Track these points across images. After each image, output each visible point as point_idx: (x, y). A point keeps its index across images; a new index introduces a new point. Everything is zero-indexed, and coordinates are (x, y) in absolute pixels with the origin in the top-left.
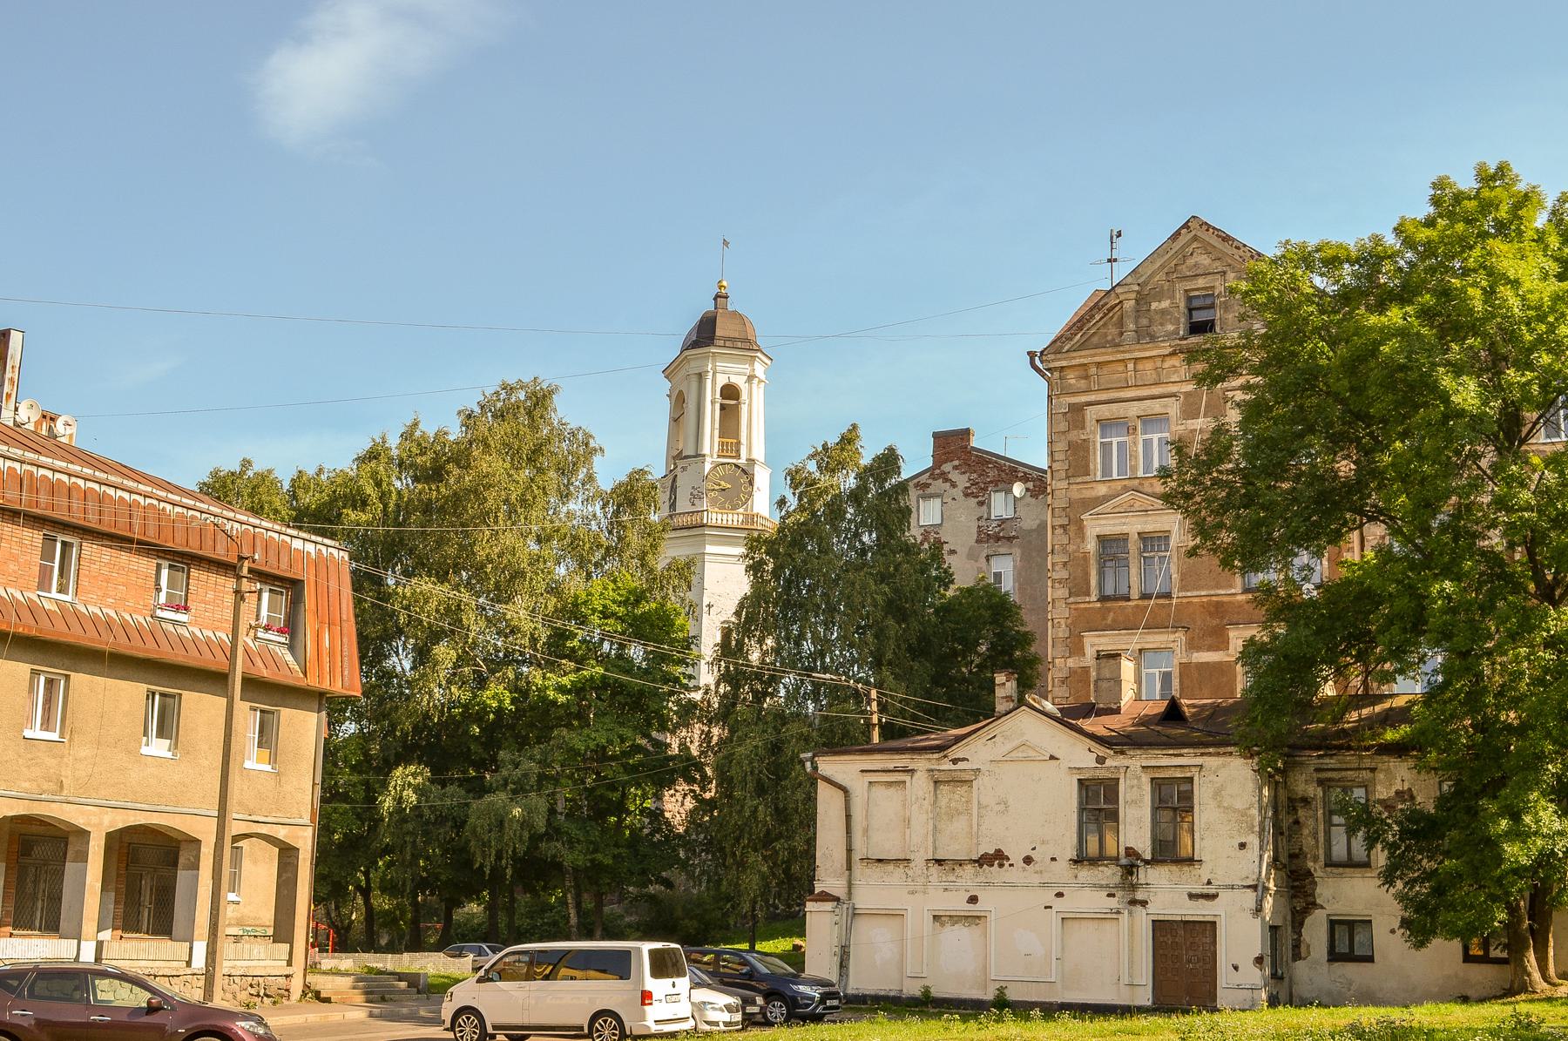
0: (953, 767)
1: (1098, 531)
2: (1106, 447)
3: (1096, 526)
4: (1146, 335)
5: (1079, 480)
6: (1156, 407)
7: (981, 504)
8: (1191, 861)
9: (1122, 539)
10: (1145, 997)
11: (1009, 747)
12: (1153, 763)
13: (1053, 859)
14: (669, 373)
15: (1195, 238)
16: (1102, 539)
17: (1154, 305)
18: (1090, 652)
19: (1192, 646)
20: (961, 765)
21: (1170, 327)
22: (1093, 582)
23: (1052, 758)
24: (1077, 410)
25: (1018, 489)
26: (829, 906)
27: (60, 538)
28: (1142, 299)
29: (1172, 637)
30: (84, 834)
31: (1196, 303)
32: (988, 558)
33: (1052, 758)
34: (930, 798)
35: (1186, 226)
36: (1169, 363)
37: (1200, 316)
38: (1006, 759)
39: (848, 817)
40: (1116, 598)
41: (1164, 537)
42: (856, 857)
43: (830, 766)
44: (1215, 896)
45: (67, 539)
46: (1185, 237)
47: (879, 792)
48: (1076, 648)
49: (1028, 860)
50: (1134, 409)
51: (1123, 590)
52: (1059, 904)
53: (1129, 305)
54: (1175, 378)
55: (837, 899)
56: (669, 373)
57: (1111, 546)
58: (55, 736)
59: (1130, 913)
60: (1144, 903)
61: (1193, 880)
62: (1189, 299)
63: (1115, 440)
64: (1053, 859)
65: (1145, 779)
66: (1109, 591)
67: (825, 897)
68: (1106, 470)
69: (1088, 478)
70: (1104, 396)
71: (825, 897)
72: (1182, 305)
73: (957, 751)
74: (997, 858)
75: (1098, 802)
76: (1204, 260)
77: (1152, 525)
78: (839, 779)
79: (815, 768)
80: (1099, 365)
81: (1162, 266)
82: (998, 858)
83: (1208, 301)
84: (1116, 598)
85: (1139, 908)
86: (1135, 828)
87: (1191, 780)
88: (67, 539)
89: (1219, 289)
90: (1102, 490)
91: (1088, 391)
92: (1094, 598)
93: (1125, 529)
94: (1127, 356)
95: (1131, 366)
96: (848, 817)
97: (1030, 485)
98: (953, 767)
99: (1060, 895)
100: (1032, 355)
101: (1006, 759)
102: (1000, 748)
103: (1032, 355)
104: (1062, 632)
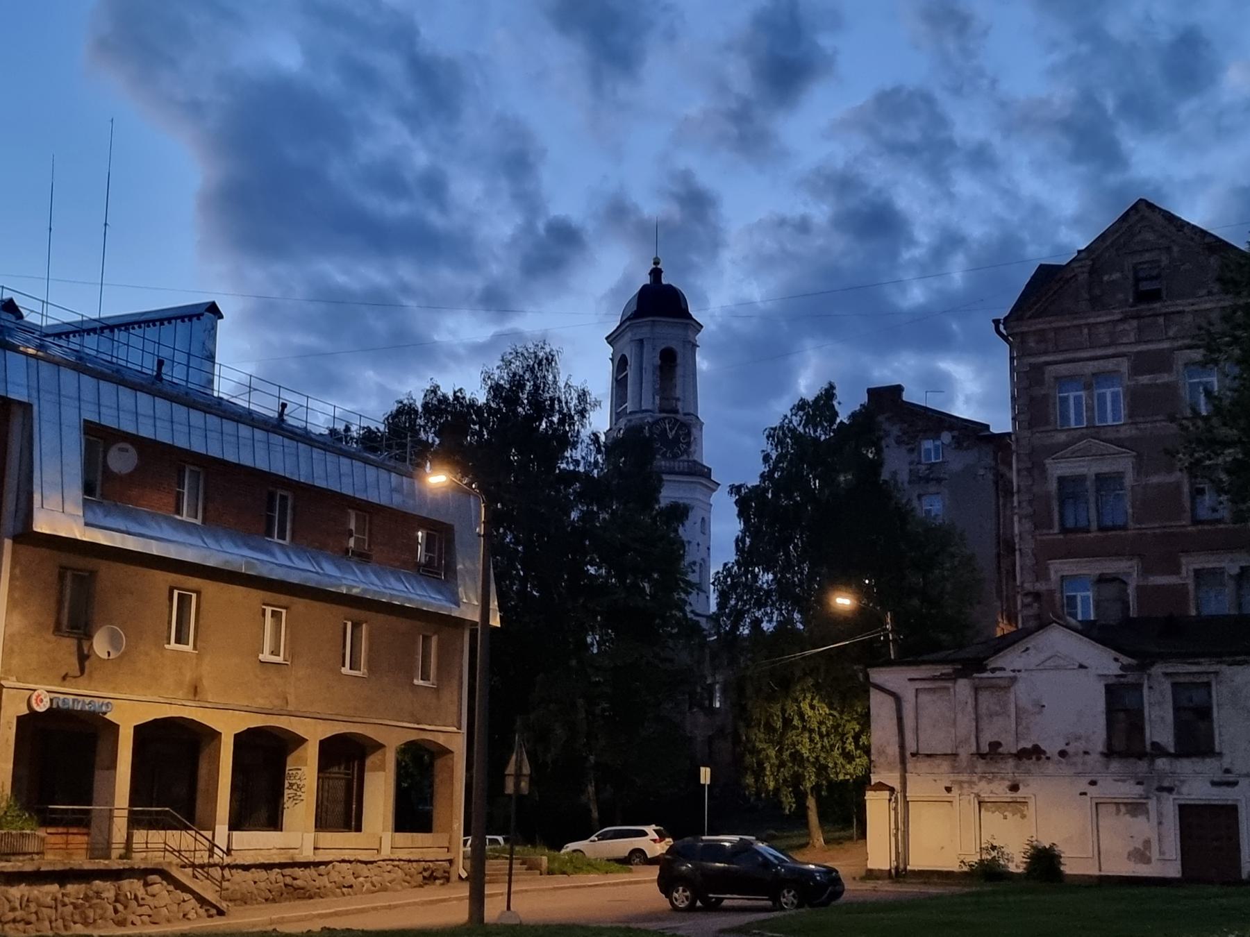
0: (991, 675)
1: (1059, 473)
2: (1064, 401)
3: (1059, 468)
4: (1097, 303)
5: (1042, 429)
6: (1110, 365)
7: (911, 451)
8: (1220, 754)
9: (1081, 479)
10: (1173, 870)
11: (1042, 657)
12: (1170, 670)
13: (1086, 753)
14: (611, 339)
15: (1143, 218)
16: (1062, 480)
17: (1106, 278)
18: (1053, 576)
19: (1146, 571)
20: (998, 674)
21: (1120, 296)
22: (1056, 517)
23: (1081, 666)
24: (1038, 369)
25: (946, 437)
26: (886, 794)
27: (280, 492)
28: (1095, 271)
29: (1129, 563)
30: (301, 741)
31: (1141, 274)
32: (919, 497)
33: (1081, 666)
34: (971, 701)
35: (1135, 207)
36: (1120, 327)
37: (1145, 286)
38: (1041, 667)
39: (900, 720)
40: (1114, 528)
41: (1120, 476)
42: (908, 754)
43: (879, 676)
44: (1235, 784)
45: (284, 493)
46: (1134, 218)
47: (924, 698)
48: (1040, 573)
49: (1063, 754)
50: (1091, 367)
51: (1083, 523)
52: (1092, 791)
53: (1083, 278)
54: (1125, 340)
55: (892, 790)
56: (611, 339)
57: (1070, 488)
58: (280, 659)
59: (1158, 799)
60: (1170, 790)
61: (1210, 767)
62: (1136, 272)
63: (1072, 395)
64: (1086, 753)
65: (1167, 686)
66: (1070, 523)
67: (881, 786)
68: (1065, 417)
69: (1050, 428)
70: (1060, 357)
71: (881, 786)
72: (1131, 276)
73: (994, 663)
74: (1036, 753)
75: (1122, 706)
76: (1150, 236)
77: (1105, 467)
78: (889, 686)
79: (867, 677)
80: (1056, 330)
81: (1112, 244)
82: (1036, 753)
83: (1155, 273)
84: (1114, 528)
85: (1165, 794)
86: (1160, 726)
87: (1208, 685)
88: (284, 493)
89: (1165, 260)
90: (1062, 437)
91: (1046, 353)
92: (1056, 530)
93: (1084, 471)
94: (1083, 322)
95: (1086, 331)
96: (900, 720)
97: (956, 433)
98: (991, 675)
99: (1093, 783)
100: (997, 322)
101: (1041, 667)
102: (1033, 659)
103: (997, 322)
104: (1029, 562)
